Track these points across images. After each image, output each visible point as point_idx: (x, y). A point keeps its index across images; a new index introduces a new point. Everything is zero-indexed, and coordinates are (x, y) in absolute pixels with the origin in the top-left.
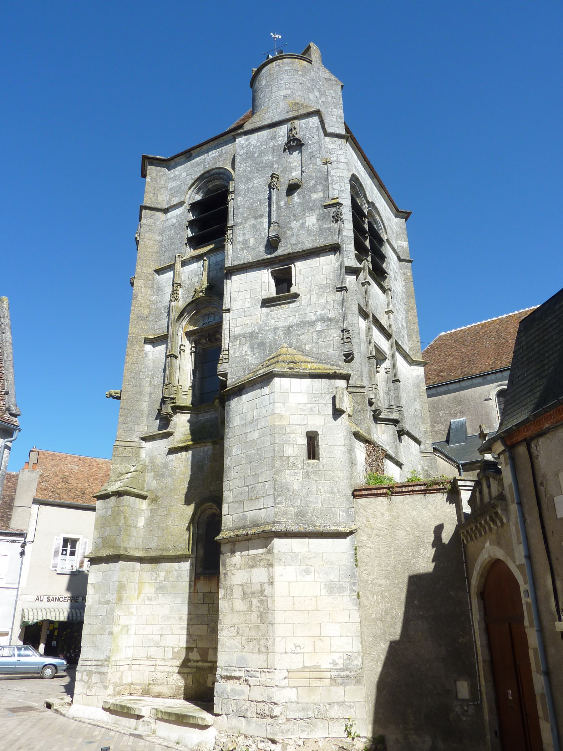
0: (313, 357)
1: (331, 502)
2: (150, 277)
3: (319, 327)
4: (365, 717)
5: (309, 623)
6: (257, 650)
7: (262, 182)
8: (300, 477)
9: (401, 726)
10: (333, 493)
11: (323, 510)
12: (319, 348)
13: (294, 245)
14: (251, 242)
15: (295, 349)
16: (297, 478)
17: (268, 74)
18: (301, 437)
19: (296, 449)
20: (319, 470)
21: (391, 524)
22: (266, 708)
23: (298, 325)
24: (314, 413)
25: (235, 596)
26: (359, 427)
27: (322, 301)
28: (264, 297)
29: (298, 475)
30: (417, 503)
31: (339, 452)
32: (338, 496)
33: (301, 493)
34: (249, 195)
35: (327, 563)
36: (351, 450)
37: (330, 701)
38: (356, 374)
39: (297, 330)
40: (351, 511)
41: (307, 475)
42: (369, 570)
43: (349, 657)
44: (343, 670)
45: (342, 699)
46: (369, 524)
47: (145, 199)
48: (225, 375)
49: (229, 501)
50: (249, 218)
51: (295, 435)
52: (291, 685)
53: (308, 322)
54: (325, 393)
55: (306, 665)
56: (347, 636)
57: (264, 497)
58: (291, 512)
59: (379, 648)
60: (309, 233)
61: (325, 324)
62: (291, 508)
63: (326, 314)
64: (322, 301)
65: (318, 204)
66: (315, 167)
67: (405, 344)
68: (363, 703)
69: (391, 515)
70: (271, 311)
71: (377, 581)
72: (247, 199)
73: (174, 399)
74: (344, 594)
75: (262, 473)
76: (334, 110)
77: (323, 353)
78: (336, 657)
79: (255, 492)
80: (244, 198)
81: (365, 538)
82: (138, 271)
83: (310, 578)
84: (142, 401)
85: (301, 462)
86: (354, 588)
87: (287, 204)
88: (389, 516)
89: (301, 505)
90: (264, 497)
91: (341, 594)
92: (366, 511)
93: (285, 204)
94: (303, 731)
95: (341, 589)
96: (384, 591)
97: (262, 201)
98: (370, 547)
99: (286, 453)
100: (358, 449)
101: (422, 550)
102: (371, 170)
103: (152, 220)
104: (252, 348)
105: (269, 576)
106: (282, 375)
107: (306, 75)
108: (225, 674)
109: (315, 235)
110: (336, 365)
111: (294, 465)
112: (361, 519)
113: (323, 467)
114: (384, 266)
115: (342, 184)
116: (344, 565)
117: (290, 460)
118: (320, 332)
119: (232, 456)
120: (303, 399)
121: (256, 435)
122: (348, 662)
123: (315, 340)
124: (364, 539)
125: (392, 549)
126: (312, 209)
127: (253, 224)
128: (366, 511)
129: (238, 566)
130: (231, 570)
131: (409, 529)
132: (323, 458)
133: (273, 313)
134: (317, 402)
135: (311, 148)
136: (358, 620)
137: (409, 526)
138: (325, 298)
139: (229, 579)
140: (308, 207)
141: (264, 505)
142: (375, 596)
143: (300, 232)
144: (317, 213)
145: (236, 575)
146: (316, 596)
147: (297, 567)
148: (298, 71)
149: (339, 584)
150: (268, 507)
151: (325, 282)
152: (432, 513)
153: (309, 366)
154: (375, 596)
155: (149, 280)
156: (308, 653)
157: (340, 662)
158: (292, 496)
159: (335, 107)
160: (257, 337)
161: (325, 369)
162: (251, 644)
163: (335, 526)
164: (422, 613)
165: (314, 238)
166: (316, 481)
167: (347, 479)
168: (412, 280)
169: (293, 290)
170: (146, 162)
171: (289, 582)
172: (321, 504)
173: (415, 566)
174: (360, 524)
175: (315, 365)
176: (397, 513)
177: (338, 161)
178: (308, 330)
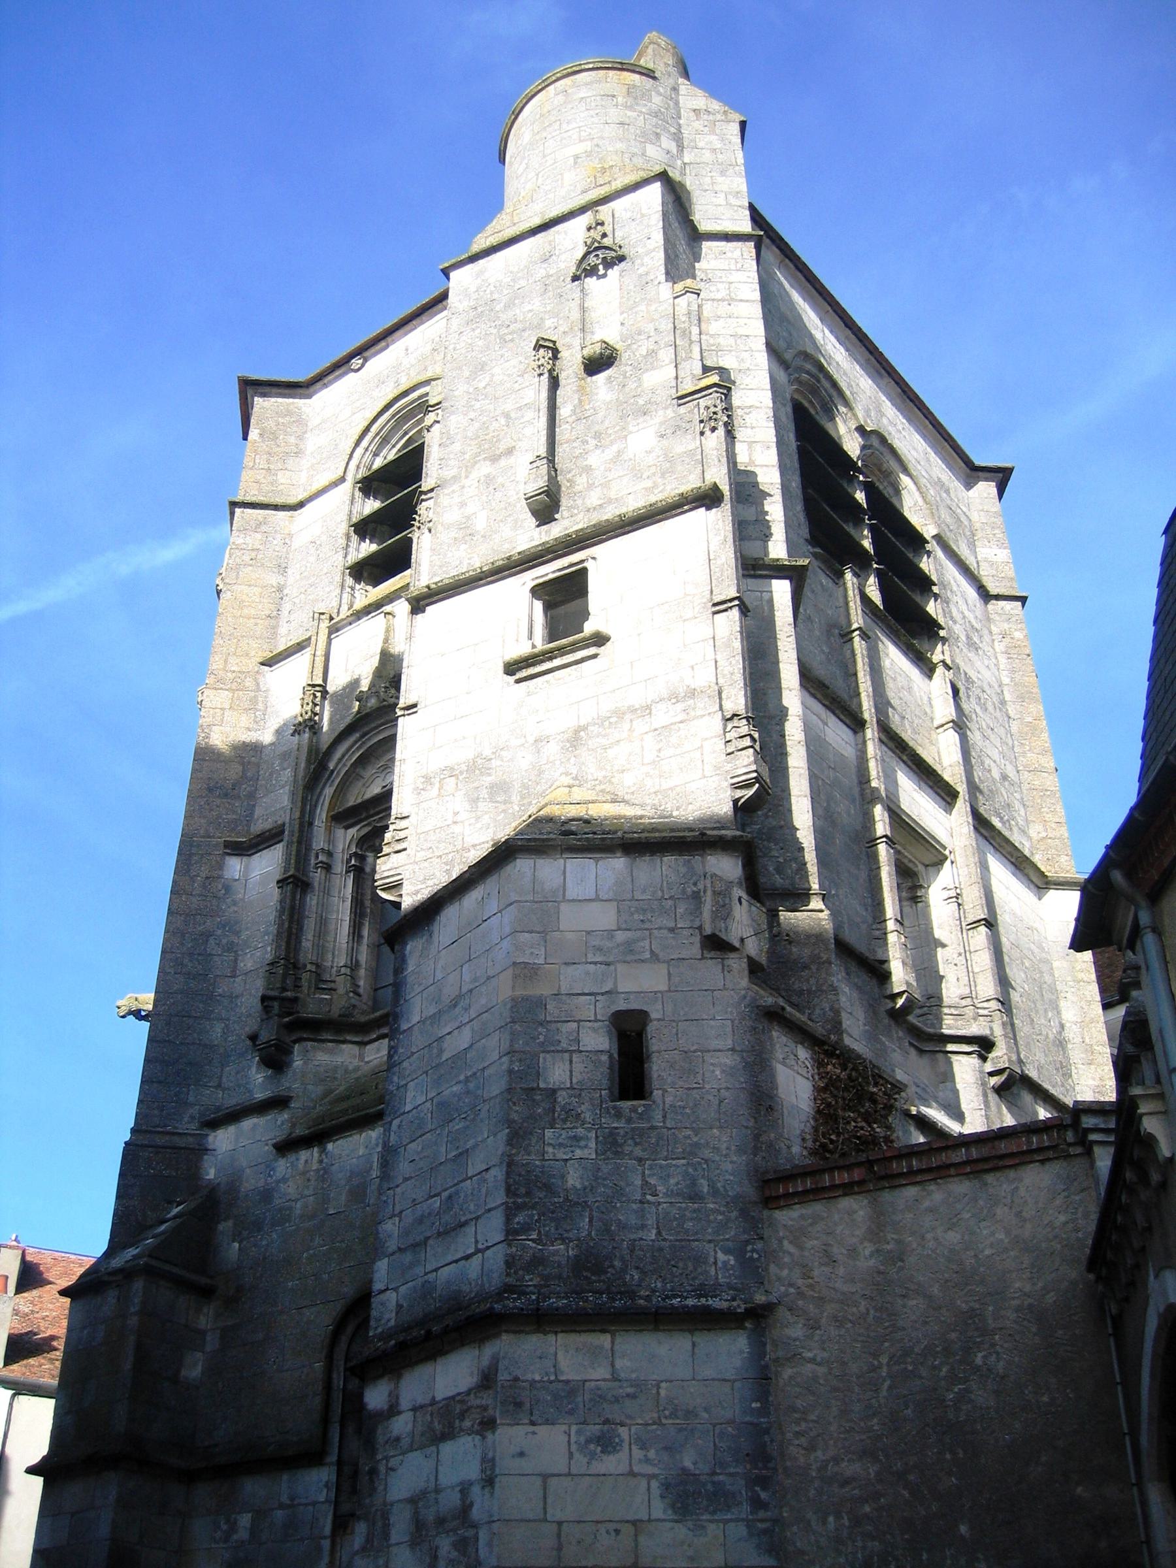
2: (249, 683)
7: (514, 367)
8: (588, 1151)
11: (661, 1249)
12: (660, 776)
13: (595, 509)
16: (578, 1153)
17: (538, 116)
18: (595, 1030)
19: (578, 1067)
20: (653, 1128)
23: (602, 721)
24: (637, 957)
25: (393, 1540)
26: (803, 1013)
29: (582, 1143)
30: (959, 1206)
32: (712, 1206)
33: (591, 1199)
34: (477, 405)
35: (674, 1415)
40: (753, 1251)
41: (611, 1144)
42: (812, 1434)
46: (811, 1287)
47: (242, 485)
48: (396, 886)
49: (390, 1250)
50: (476, 463)
51: (575, 1024)
54: (671, 898)
57: (477, 1218)
58: (557, 1258)
66: (653, 308)
67: (1015, 829)
69: (878, 1251)
70: (529, 694)
71: (836, 1469)
72: (472, 415)
73: (295, 1000)
74: (729, 1517)
75: (476, 1146)
76: (720, 179)
81: (797, 1331)
82: (215, 667)
83: (612, 1464)
84: (209, 1019)
85: (593, 1105)
86: (763, 1495)
87: (578, 411)
88: (871, 1256)
89: (590, 1234)
90: (477, 1218)
92: (801, 1248)
93: (574, 412)
95: (719, 1499)
97: (513, 415)
98: (812, 1360)
99: (545, 1081)
100: (784, 1064)
101: (980, 1355)
102: (871, 353)
103: (258, 536)
105: (484, 1460)
107: (637, 104)
109: (654, 474)
111: (571, 1115)
112: (785, 1272)
113: (664, 1117)
114: (932, 608)
115: (745, 355)
116: (730, 1422)
117: (560, 1099)
118: (661, 732)
119: (404, 1113)
120: (604, 918)
121: (463, 1039)
124: (794, 1335)
125: (884, 1360)
127: (487, 476)
128: (801, 1248)
129: (405, 1442)
130: (387, 1458)
131: (935, 1290)
135: (643, 265)
139: (381, 1487)
141: (477, 1242)
142: (831, 1519)
144: (657, 420)
145: (400, 1471)
146: (634, 1523)
147: (574, 1428)
148: (614, 96)
149: (713, 1483)
150: (488, 1248)
152: (1008, 1232)
154: (831, 1519)
155: (244, 689)
158: (561, 1207)
159: (723, 173)
163: (699, 1296)
165: (649, 483)
166: (640, 1160)
168: (1028, 652)
170: (250, 392)
171: (545, 1477)
172: (654, 1231)
174: (783, 1289)
177: (732, 299)
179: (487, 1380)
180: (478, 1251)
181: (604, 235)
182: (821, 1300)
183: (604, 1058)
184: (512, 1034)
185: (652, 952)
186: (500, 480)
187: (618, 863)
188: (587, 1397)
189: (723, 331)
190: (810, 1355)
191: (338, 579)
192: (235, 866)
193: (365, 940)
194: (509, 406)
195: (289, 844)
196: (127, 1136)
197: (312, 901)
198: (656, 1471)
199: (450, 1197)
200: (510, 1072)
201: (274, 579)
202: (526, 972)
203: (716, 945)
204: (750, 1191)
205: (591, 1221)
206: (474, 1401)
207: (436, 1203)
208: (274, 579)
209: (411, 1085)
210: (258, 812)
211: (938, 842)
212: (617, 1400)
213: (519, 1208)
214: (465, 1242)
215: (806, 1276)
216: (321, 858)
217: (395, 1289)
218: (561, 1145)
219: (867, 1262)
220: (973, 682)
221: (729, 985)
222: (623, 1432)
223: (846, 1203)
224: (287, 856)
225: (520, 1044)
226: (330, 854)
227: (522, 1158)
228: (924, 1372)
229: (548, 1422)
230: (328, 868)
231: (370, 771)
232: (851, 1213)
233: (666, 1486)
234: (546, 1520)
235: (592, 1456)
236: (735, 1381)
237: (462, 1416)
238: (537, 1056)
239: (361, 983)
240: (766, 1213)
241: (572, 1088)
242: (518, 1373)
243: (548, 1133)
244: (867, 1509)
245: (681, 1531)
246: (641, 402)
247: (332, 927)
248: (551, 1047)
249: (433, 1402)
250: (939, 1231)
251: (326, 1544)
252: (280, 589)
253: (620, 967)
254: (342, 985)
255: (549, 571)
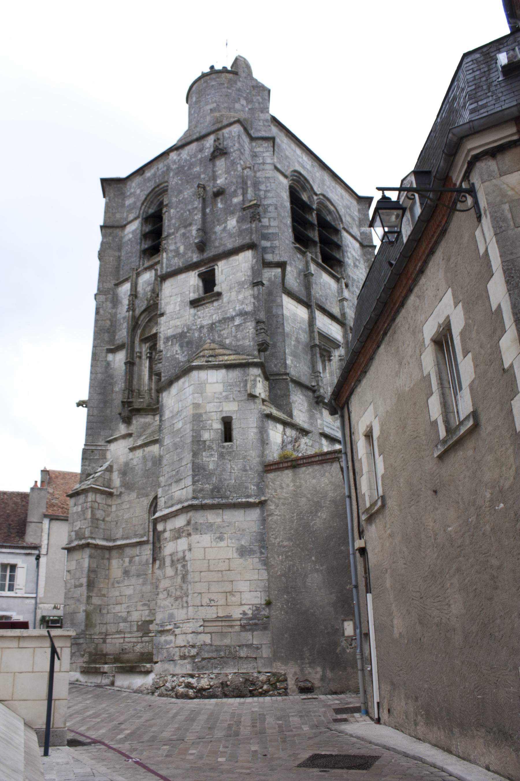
0: (232, 350)
1: (244, 478)
3: (237, 321)
4: (271, 656)
5: (222, 581)
6: (181, 606)
9: (299, 661)
10: (245, 470)
11: (236, 485)
14: (182, 249)
15: (217, 344)
16: (212, 459)
18: (217, 423)
20: (233, 451)
21: (295, 493)
22: (186, 651)
23: (220, 321)
27: (241, 297)
28: (191, 299)
30: (316, 473)
31: (252, 434)
34: (180, 206)
35: (239, 530)
36: (262, 432)
37: (239, 644)
38: (280, 363)
39: (219, 326)
41: (222, 456)
43: (257, 609)
44: (251, 619)
45: (250, 642)
52: (206, 631)
53: (228, 318)
55: (219, 615)
56: (256, 591)
59: (283, 599)
60: (231, 235)
61: (243, 318)
62: (207, 486)
63: (243, 308)
64: (241, 297)
65: (238, 207)
68: (269, 645)
70: (198, 311)
72: (178, 210)
75: (184, 457)
77: (240, 345)
78: (246, 608)
79: (179, 475)
80: (176, 209)
81: (273, 507)
83: (223, 544)
86: (263, 551)
91: (251, 556)
92: (274, 484)
93: (210, 211)
94: (216, 668)
95: (251, 552)
96: (288, 552)
97: (191, 211)
100: (272, 430)
104: (181, 346)
106: (199, 368)
108: (160, 629)
110: (251, 355)
111: (210, 448)
112: (270, 491)
115: (268, 184)
116: (255, 532)
120: (219, 388)
122: (256, 612)
123: (234, 334)
125: (295, 514)
126: (232, 213)
128: (274, 484)
129: (168, 539)
130: (163, 544)
131: (309, 496)
132: (237, 440)
133: (199, 313)
134: (232, 390)
136: (267, 578)
137: (309, 493)
138: (243, 294)
140: (229, 211)
142: (280, 557)
143: (223, 235)
146: (229, 559)
147: (212, 535)
151: (243, 279)
152: (328, 480)
153: (226, 358)
154: (280, 557)
156: (221, 606)
157: (250, 612)
160: (186, 337)
161: (239, 360)
162: (177, 602)
164: (317, 567)
165: (234, 239)
166: (230, 460)
167: (259, 457)
169: (216, 289)
171: (205, 548)
173: (313, 528)
175: (232, 357)
176: (300, 482)
178: (228, 325)
179: (189, 523)
180: (185, 487)
181: (220, 144)
182: (279, 498)
183: (219, 431)
184: (193, 424)
185: (233, 398)
186: (187, 235)
187: (223, 371)
188: (216, 526)
189: (261, 176)
190: (276, 513)
191: (138, 255)
192: (110, 357)
193: (154, 381)
194: (190, 207)
195: (127, 350)
196: (83, 447)
197: (136, 368)
198: (234, 545)
199: (178, 471)
200: (193, 436)
201: (117, 254)
202: (196, 406)
203: (252, 397)
204: (260, 468)
205: (216, 478)
206: (185, 528)
207: (174, 473)
208: (117, 254)
209: (166, 437)
210: (117, 337)
211: (338, 341)
212: (224, 527)
213: (196, 475)
214: (182, 485)
215: (276, 492)
216: (138, 354)
217: (164, 497)
218: (208, 457)
219: (291, 488)
220: (355, 280)
221: (256, 408)
222: (226, 535)
223: (286, 472)
224: (127, 353)
225: (195, 428)
226: (141, 353)
227: (197, 461)
228: (305, 518)
229: (205, 534)
230: (140, 357)
231: (152, 324)
232: (288, 474)
233: (237, 549)
234: (205, 559)
235: (217, 542)
236: (255, 521)
237: (183, 532)
238: (200, 431)
239: (153, 395)
240: (265, 474)
241: (210, 440)
242: (197, 521)
243: (204, 453)
244: (290, 554)
245: (241, 561)
246: (232, 209)
247: (142, 377)
248: (204, 428)
249: (175, 529)
250: (311, 480)
251: (151, 566)
252: (119, 257)
253: (224, 403)
254: (147, 397)
255: (203, 269)
